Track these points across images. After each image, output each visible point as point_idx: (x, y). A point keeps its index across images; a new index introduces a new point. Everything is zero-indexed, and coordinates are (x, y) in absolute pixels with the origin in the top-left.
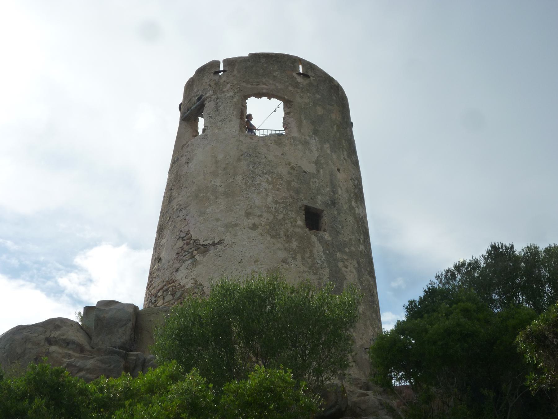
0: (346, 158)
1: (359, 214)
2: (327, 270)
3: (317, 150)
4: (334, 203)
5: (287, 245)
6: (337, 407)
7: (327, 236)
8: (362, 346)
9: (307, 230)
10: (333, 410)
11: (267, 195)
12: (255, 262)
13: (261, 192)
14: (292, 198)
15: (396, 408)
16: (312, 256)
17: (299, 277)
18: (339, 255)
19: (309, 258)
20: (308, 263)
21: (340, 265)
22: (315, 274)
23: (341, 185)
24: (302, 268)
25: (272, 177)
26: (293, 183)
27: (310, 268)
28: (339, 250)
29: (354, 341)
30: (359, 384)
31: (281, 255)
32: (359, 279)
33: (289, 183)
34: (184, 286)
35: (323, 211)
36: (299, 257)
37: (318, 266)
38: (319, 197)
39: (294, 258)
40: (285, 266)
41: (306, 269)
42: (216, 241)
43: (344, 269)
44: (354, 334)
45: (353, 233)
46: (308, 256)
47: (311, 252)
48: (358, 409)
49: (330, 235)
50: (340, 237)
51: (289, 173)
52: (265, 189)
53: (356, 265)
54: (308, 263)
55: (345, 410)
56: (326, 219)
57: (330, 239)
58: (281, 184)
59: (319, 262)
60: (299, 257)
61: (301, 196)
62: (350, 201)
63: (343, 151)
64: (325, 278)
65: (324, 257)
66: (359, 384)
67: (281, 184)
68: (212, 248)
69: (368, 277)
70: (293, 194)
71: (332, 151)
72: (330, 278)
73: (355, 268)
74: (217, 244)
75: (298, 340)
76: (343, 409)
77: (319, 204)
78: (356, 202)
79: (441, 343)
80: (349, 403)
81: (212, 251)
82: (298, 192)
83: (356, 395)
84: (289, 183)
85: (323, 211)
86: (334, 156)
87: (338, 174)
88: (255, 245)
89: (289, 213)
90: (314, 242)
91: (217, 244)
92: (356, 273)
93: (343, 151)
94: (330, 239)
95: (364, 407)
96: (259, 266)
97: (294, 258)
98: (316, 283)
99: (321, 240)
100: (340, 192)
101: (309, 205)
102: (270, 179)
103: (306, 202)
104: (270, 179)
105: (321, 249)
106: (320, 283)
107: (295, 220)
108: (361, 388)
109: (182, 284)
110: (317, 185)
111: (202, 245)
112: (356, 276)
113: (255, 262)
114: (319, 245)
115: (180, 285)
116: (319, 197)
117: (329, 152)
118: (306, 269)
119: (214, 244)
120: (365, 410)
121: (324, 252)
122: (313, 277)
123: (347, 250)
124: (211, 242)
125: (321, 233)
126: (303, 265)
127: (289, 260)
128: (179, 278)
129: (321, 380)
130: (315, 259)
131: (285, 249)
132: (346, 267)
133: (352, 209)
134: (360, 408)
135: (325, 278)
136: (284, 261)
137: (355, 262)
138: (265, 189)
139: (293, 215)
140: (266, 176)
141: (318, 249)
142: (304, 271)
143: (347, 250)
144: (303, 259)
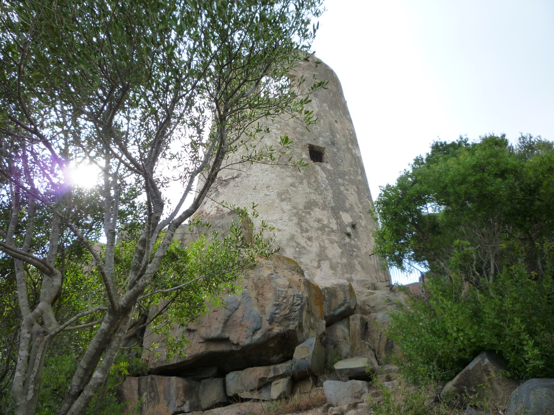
0: (342, 114)
1: (355, 154)
2: (331, 191)
3: (318, 106)
4: (333, 143)
5: (294, 173)
6: (346, 305)
7: (329, 167)
8: (366, 253)
9: (312, 162)
10: (343, 308)
11: (277, 138)
12: (267, 187)
13: (272, 136)
14: (298, 139)
15: (404, 303)
16: (316, 181)
17: (306, 197)
18: (340, 180)
19: (314, 182)
20: (313, 186)
21: (342, 188)
22: (320, 195)
23: (339, 132)
24: (308, 190)
25: (281, 125)
26: (298, 129)
27: (316, 190)
28: (340, 177)
29: (359, 250)
30: (366, 284)
31: (290, 180)
32: (360, 200)
33: (295, 129)
34: (209, 214)
35: (325, 148)
36: (305, 182)
37: (322, 188)
38: (321, 139)
39: (301, 183)
40: (294, 189)
41: (312, 191)
42: (235, 175)
43: (346, 192)
44: (359, 243)
45: (351, 166)
46: (313, 181)
47: (316, 177)
48: (367, 307)
49: (332, 166)
50: (341, 168)
51: (294, 122)
52: (275, 134)
53: (356, 190)
54: (313, 186)
55: (355, 308)
56: (327, 154)
57: (331, 168)
58: (288, 130)
59: (323, 185)
60: (305, 182)
61: (306, 137)
62: (347, 144)
63: (339, 110)
64: (329, 198)
65: (327, 181)
66: (366, 284)
67: (288, 130)
68: (232, 181)
69: (367, 199)
70: (299, 136)
71: (329, 108)
72: (333, 198)
73: (355, 192)
74: (236, 177)
75: (169, 137)
76: (353, 307)
77: (320, 143)
78: (352, 145)
79: (473, 179)
80: (359, 303)
81: (232, 183)
82: (302, 134)
83: (365, 295)
84: (295, 129)
85: (325, 148)
86: (332, 112)
87: (336, 124)
88: (267, 175)
89: (296, 149)
90: (318, 171)
91: (236, 177)
92: (356, 195)
93: (339, 110)
94: (331, 168)
95: (372, 304)
96: (271, 190)
97: (301, 183)
98: (322, 201)
99: (324, 169)
100: (338, 136)
101: (313, 143)
102: (279, 127)
103: (309, 142)
104: (279, 127)
105: (325, 175)
106: (324, 202)
107: (301, 155)
108: (368, 288)
109: (208, 213)
110: (319, 130)
111: (224, 180)
112: (357, 197)
113: (267, 187)
114: (322, 172)
115: (206, 213)
116: (321, 139)
117: (327, 109)
118: (312, 191)
119: (233, 178)
120: (373, 307)
121: (327, 178)
122: (318, 197)
123: (347, 177)
124: (230, 177)
125: (324, 164)
126: (309, 188)
127: (297, 184)
128: (206, 208)
129: (23, 96)
130: (320, 183)
131: (293, 176)
132: (347, 190)
133: (349, 149)
134: (369, 306)
135: (329, 198)
136: (292, 185)
137: (355, 187)
138: (275, 134)
139: (299, 151)
140: (276, 125)
141: (322, 175)
142: (310, 193)
143: (347, 177)
144: (309, 183)
